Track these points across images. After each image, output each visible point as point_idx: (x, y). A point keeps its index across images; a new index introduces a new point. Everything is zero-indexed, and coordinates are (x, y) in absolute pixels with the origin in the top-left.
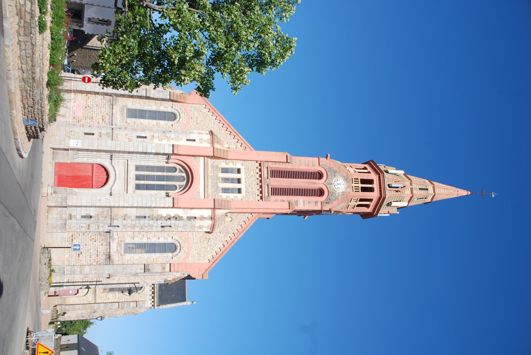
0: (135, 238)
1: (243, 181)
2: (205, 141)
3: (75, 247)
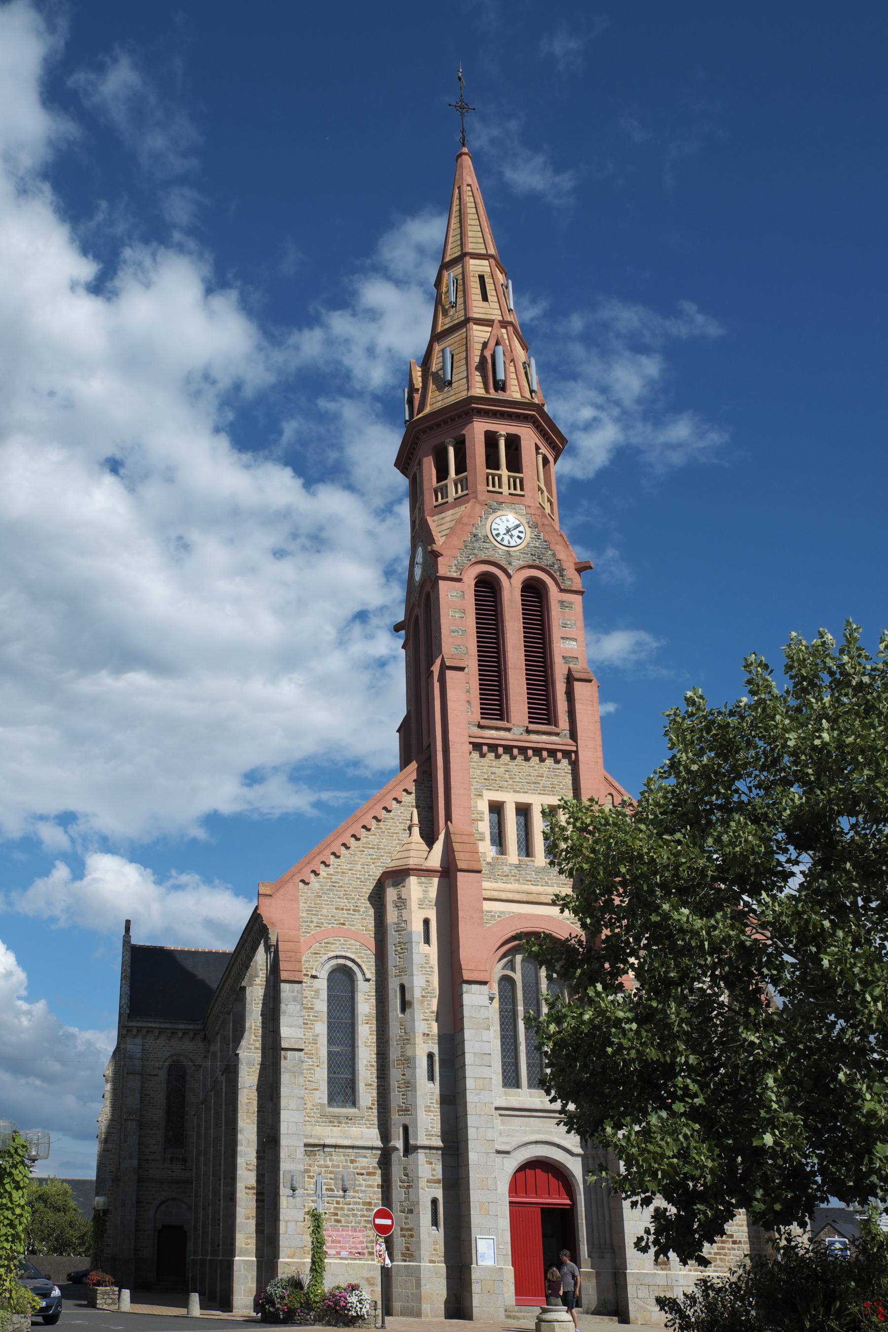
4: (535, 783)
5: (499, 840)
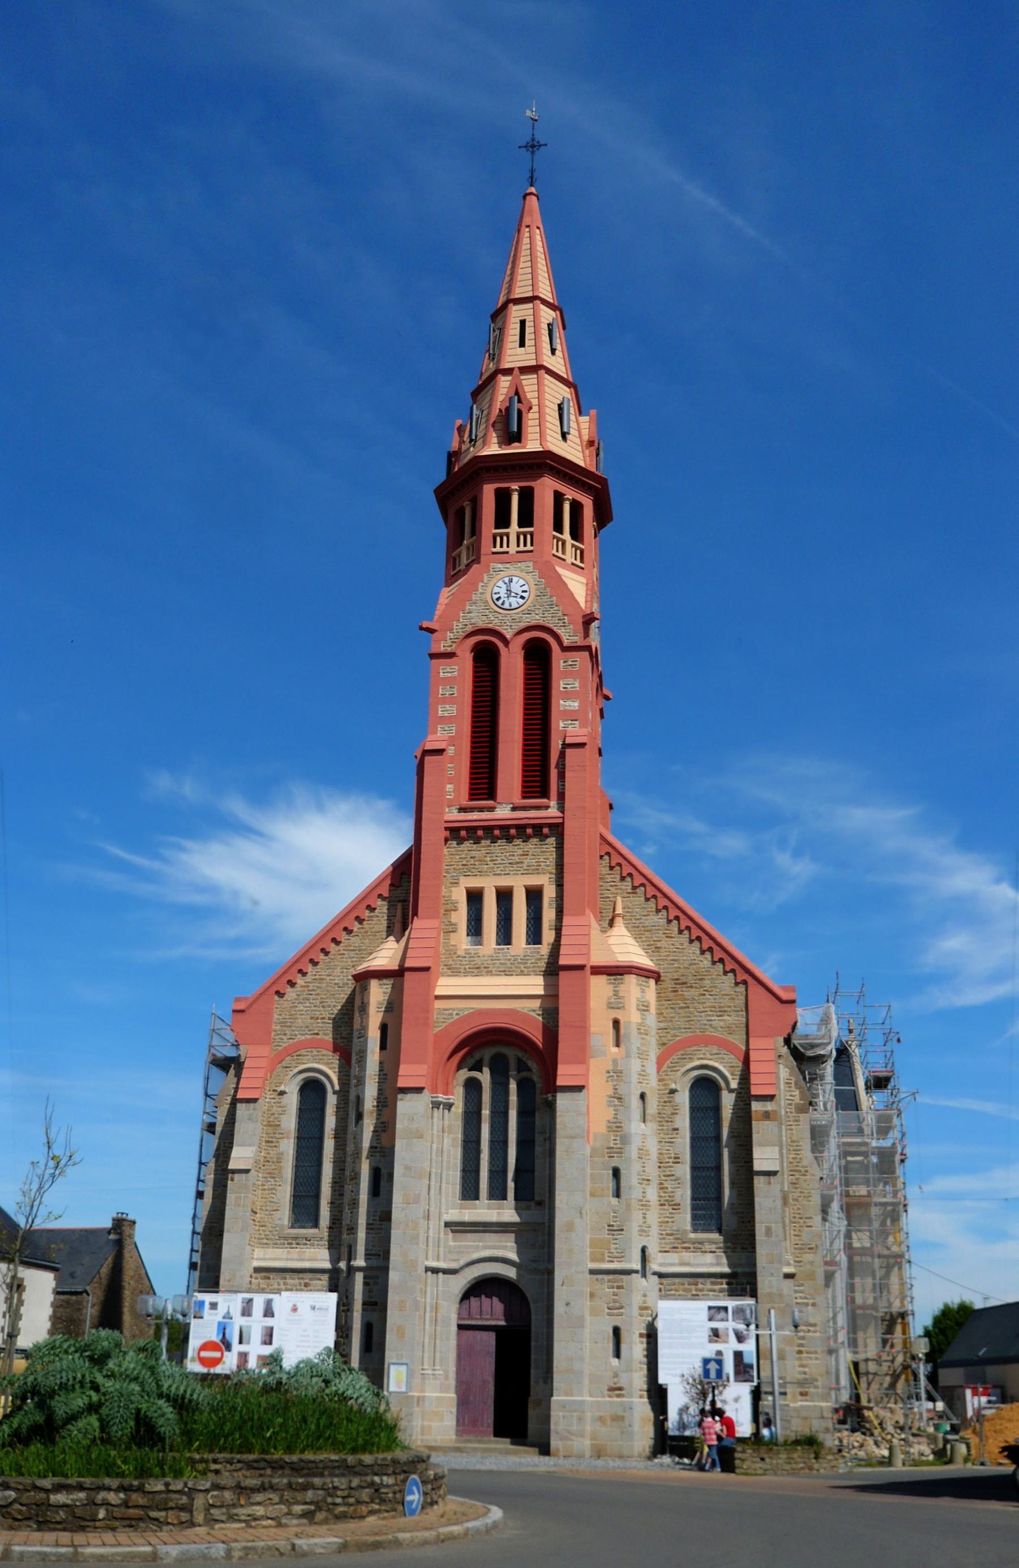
0: (677, 1200)
1: (504, 882)
2: (616, 993)
3: (713, 1374)
4: (517, 863)
5: (475, 928)
